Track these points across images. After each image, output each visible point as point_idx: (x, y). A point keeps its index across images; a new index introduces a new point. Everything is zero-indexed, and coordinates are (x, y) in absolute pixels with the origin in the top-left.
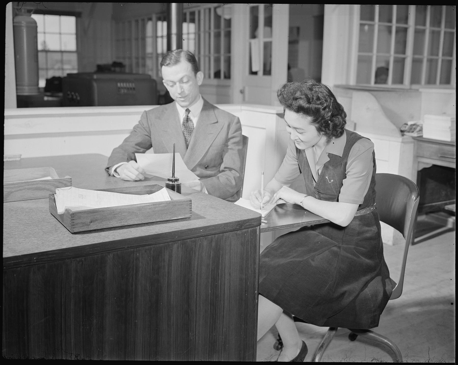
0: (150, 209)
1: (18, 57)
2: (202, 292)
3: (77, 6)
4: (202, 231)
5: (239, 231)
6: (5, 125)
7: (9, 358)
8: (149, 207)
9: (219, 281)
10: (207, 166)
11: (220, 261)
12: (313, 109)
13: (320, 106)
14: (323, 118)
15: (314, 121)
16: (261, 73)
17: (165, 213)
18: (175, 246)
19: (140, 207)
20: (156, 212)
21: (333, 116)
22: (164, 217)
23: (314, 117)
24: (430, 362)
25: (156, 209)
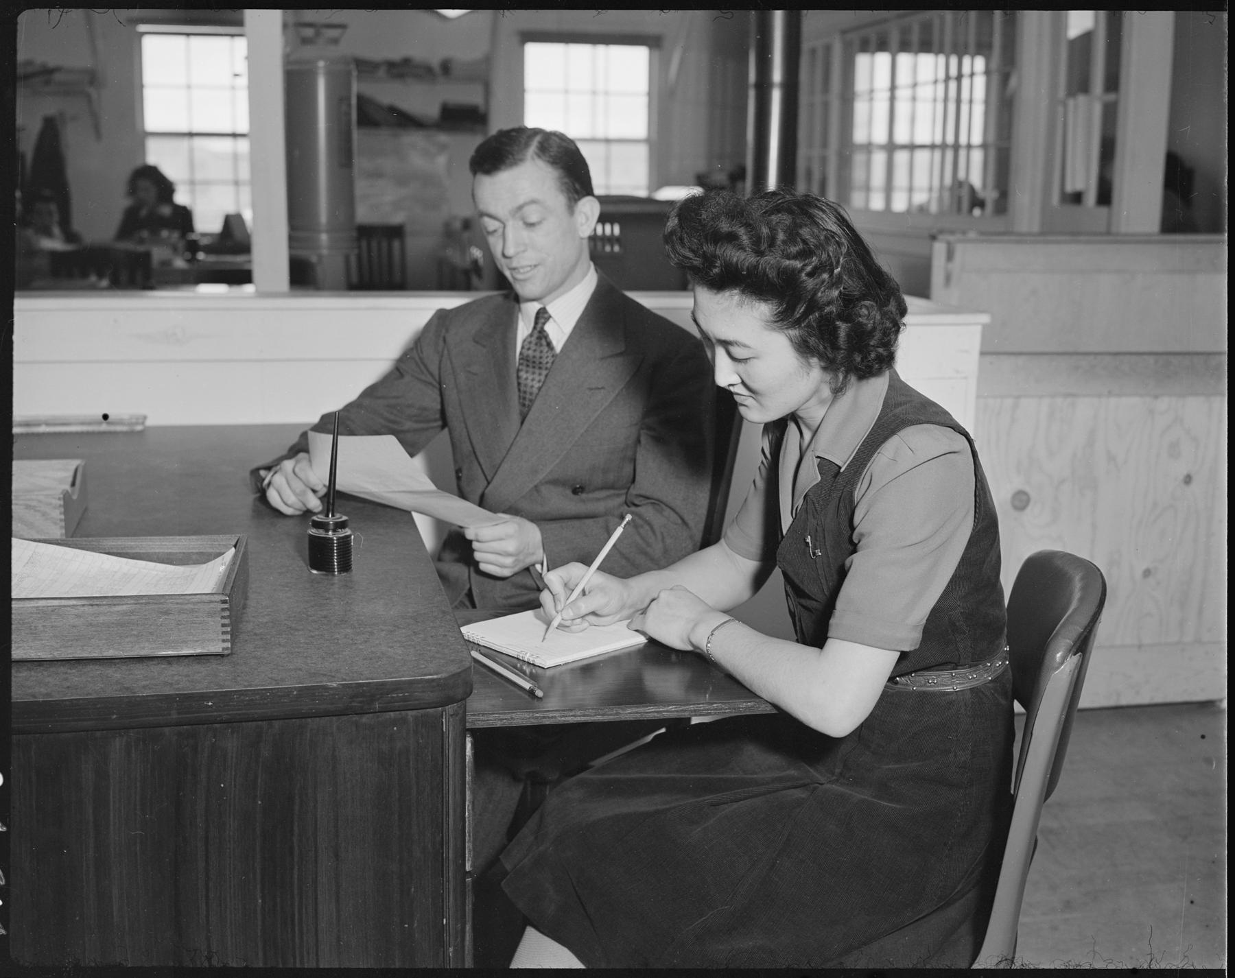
0: (78, 616)
1: (297, 153)
2: (228, 899)
3: (650, 19)
4: (210, 704)
5: (367, 716)
6: (15, 338)
7: (28, 964)
8: (74, 611)
9: (296, 871)
10: (580, 487)
11: (297, 808)
12: (772, 274)
13: (798, 264)
14: (813, 306)
15: (784, 318)
16: (1091, 198)
17: (134, 635)
18: (118, 744)
19: (44, 607)
20: (99, 629)
21: (848, 301)
22: (130, 645)
23: (780, 304)
24: (1153, 967)
25: (101, 619)
